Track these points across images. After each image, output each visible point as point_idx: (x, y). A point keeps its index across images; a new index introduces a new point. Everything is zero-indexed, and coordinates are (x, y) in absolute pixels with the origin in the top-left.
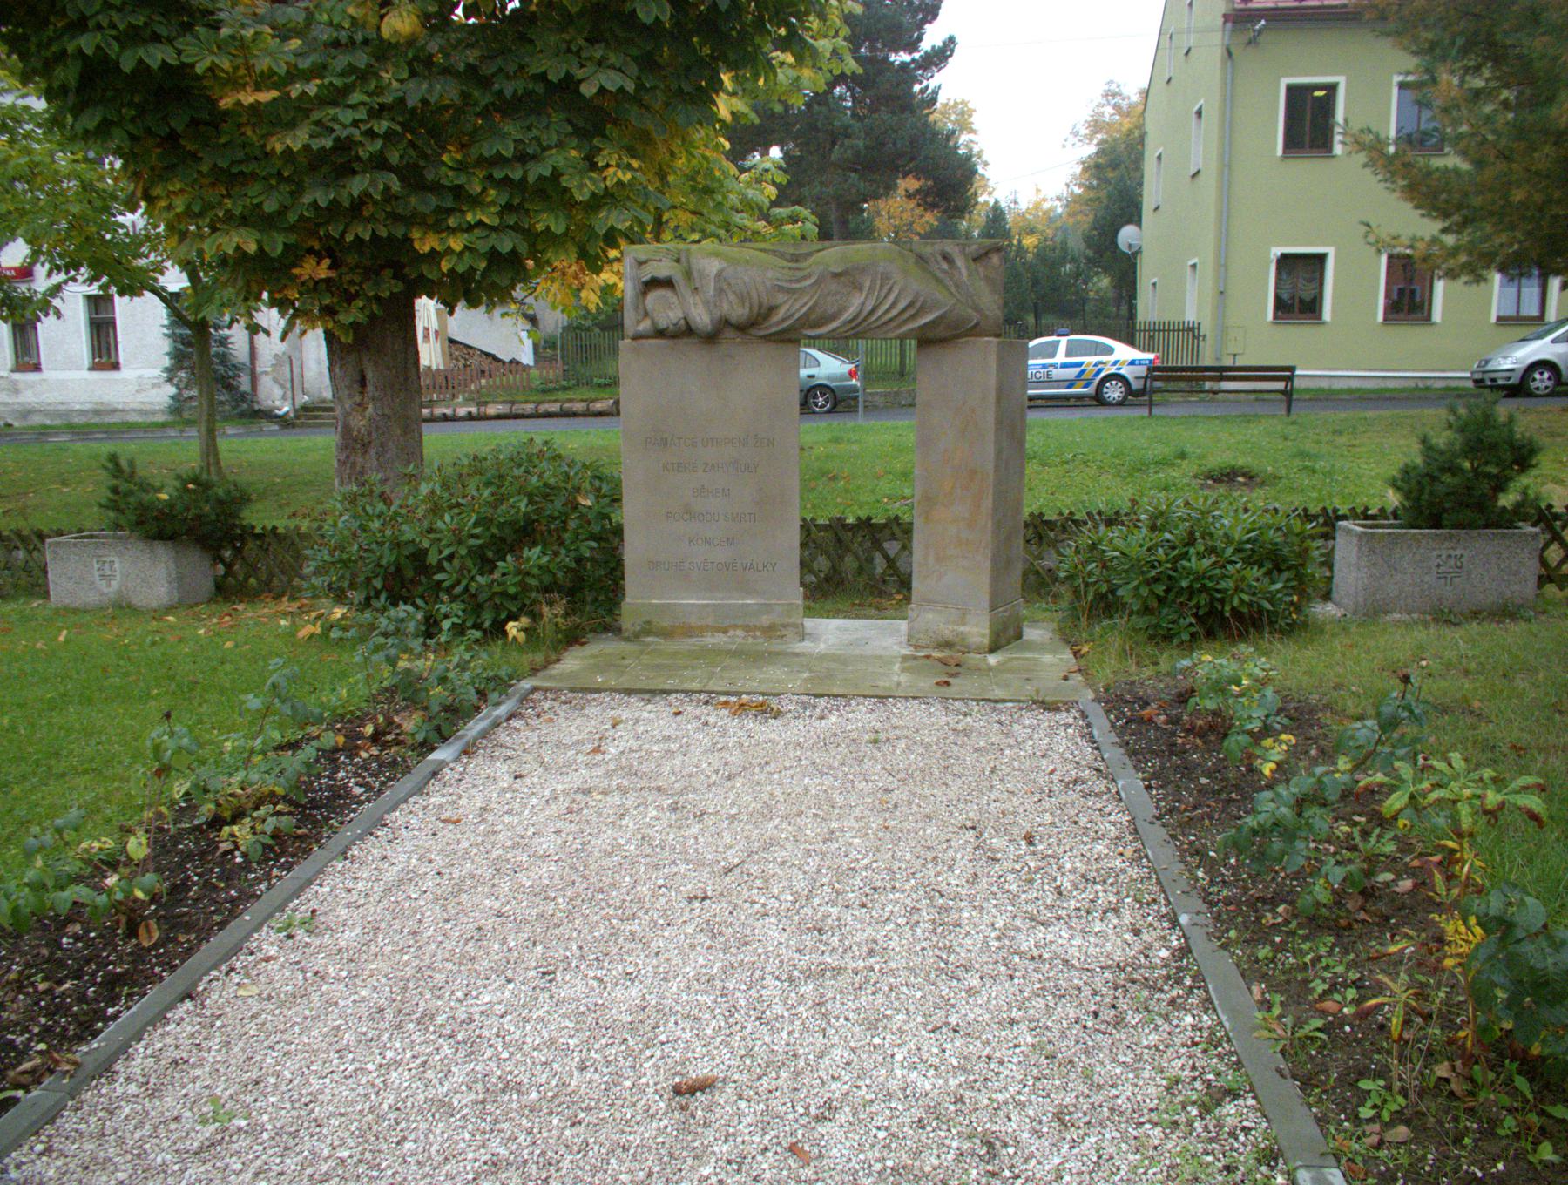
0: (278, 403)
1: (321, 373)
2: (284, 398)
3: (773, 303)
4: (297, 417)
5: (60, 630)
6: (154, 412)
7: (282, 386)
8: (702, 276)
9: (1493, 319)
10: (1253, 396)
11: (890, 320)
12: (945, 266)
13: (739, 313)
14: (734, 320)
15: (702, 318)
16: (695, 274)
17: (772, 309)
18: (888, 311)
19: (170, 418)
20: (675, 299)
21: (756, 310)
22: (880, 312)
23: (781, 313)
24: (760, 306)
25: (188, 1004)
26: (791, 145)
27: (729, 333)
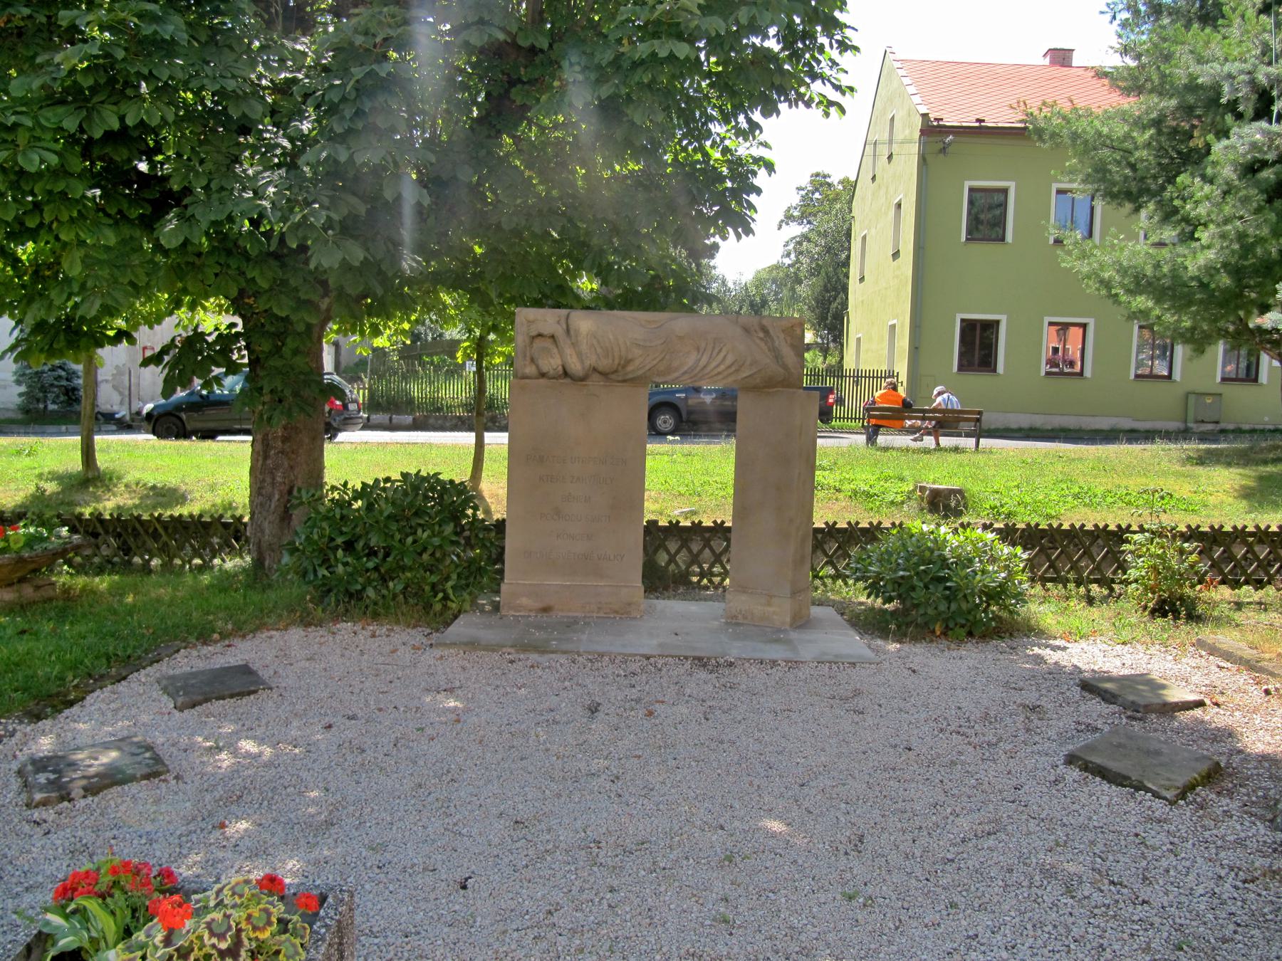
0: (115, 408)
1: (154, 384)
2: (121, 403)
3: (630, 357)
4: (133, 420)
5: (358, 510)
6: (7, 410)
7: (121, 394)
8: (577, 332)
9: (1218, 379)
10: (127, 393)
11: (719, 373)
12: (761, 335)
13: (604, 364)
14: (600, 369)
15: (576, 367)
16: (572, 332)
17: (629, 361)
18: (718, 366)
19: (20, 416)
20: (555, 350)
21: (616, 362)
22: (709, 368)
23: (637, 363)
24: (620, 357)
25: (66, 803)
26: (814, 360)
27: (596, 377)
